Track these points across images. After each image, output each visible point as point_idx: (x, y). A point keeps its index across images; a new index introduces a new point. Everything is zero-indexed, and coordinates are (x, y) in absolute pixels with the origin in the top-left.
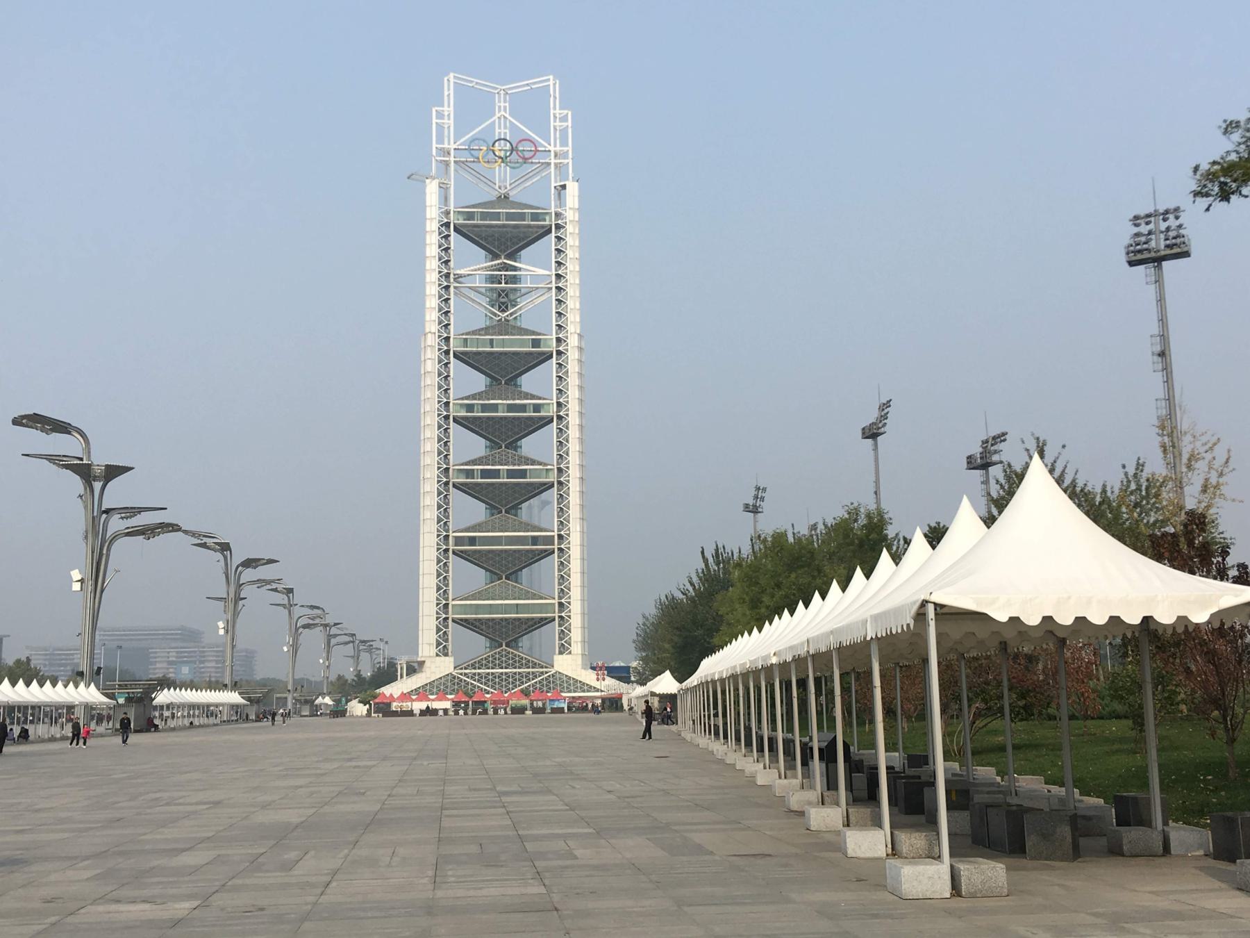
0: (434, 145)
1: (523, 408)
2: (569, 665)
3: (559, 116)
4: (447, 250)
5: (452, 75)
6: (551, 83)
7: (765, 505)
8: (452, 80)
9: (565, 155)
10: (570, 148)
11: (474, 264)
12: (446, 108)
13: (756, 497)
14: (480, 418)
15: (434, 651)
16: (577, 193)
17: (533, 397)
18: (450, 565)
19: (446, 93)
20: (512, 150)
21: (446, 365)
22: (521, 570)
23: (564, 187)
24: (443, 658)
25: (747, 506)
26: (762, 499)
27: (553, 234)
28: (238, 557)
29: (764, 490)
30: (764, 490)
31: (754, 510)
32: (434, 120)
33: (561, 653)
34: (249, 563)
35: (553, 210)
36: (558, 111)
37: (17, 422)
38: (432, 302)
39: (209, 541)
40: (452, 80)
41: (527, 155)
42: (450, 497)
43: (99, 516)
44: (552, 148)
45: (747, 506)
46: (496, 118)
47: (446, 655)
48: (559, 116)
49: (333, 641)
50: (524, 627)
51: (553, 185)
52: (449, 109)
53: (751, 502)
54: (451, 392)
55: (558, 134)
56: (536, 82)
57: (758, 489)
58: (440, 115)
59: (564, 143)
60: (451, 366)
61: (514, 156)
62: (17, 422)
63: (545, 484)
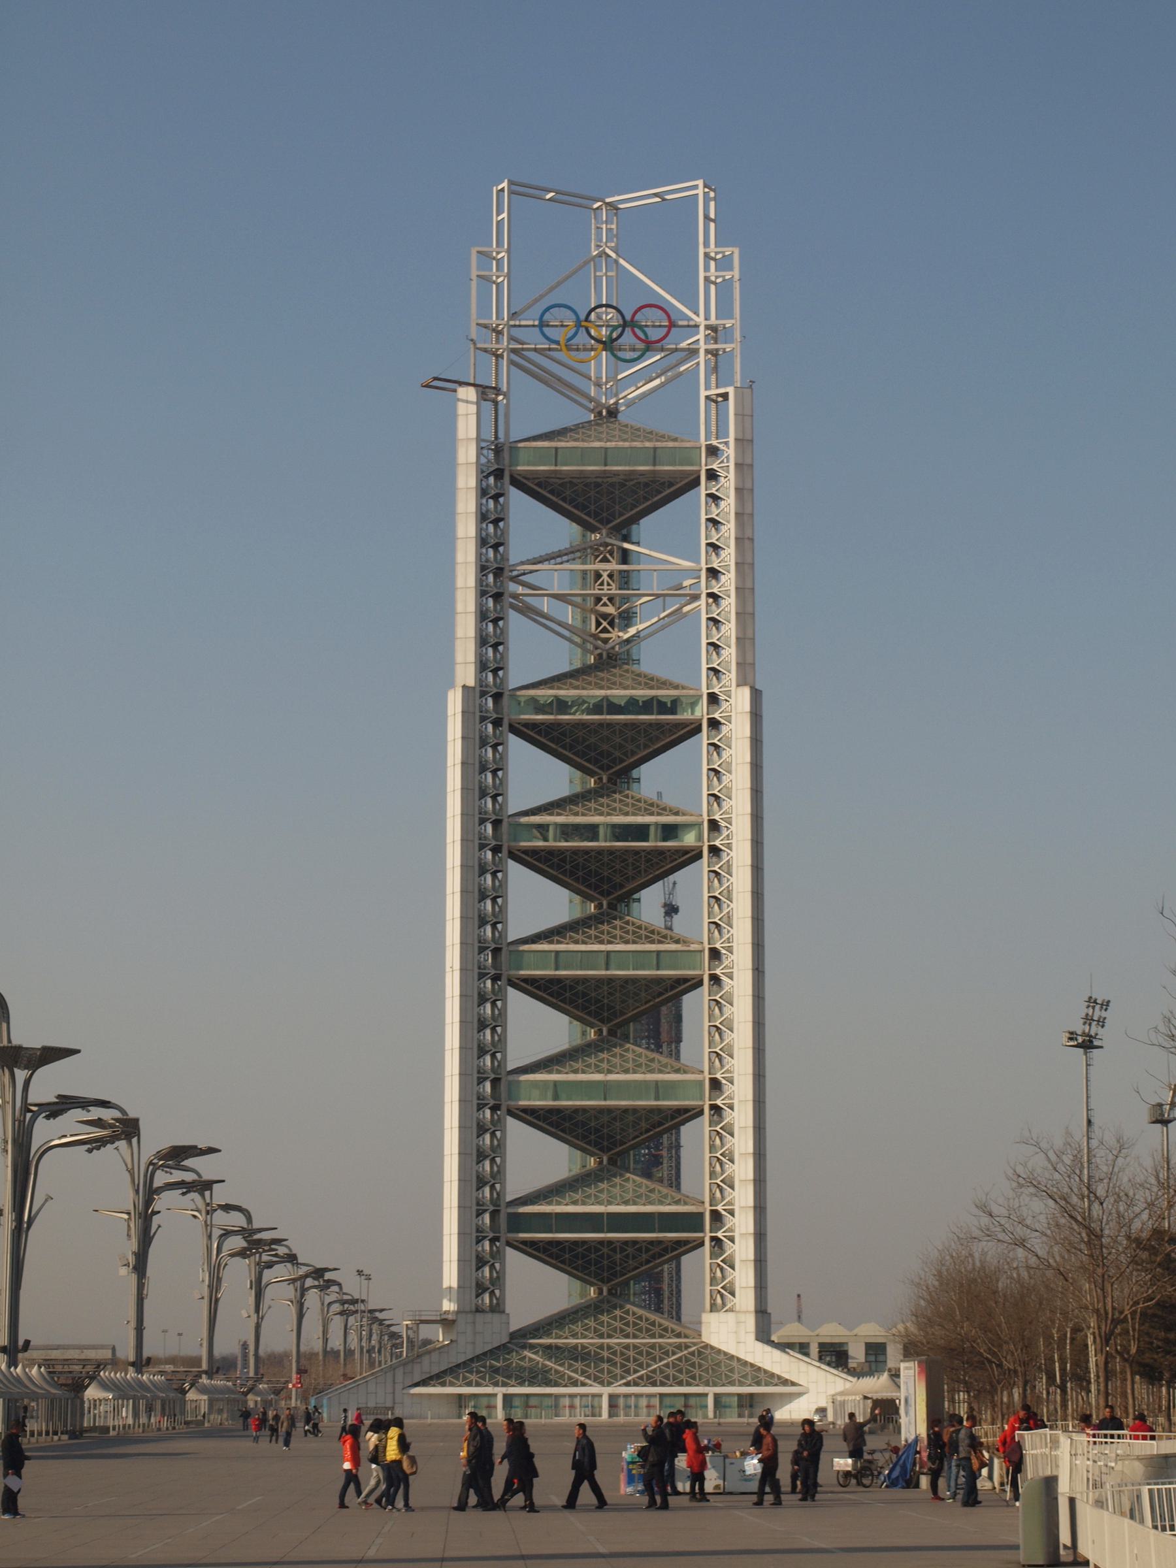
1: (641, 832)
2: (729, 1331)
3: (714, 259)
6: (700, 191)
7: (1105, 1036)
11: (536, 528)
13: (1088, 1020)
14: (561, 852)
17: (664, 810)
20: (625, 325)
25: (1072, 1036)
26: (1101, 1022)
27: (703, 490)
28: (153, 1141)
29: (1106, 1005)
30: (1106, 1005)
31: (1088, 1045)
33: (714, 1308)
34: (177, 1155)
35: (703, 442)
37: (78, 1051)
38: (466, 627)
41: (654, 334)
44: (700, 319)
45: (1072, 1036)
48: (714, 259)
49: (267, 1275)
50: (644, 1256)
51: (703, 393)
53: (1079, 1028)
55: (709, 294)
56: (675, 191)
57: (1092, 1002)
58: (485, 255)
61: (628, 338)
62: (78, 1051)
63: (685, 980)
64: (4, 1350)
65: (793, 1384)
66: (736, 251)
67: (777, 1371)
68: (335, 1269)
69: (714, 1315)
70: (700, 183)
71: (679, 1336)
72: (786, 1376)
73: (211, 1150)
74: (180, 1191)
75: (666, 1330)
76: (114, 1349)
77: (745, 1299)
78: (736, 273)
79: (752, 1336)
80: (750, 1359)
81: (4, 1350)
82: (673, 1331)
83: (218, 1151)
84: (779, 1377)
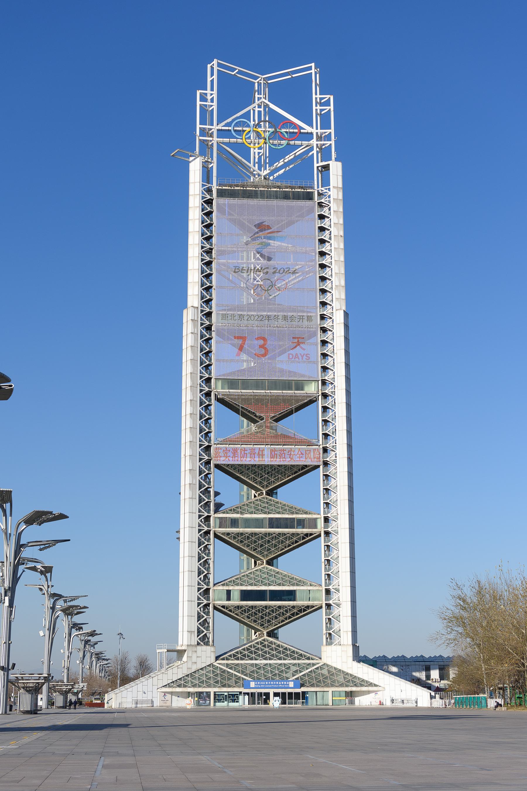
0: (198, 126)
2: (337, 656)
4: (208, 354)
5: (215, 62)
6: (313, 71)
8: (216, 68)
9: (328, 137)
10: (332, 131)
12: (209, 91)
15: (195, 639)
16: (340, 173)
18: (211, 547)
19: (209, 79)
21: (207, 407)
22: (276, 557)
23: (326, 168)
24: (204, 648)
32: (198, 103)
36: (318, 96)
39: (39, 566)
40: (216, 68)
42: (211, 476)
43: (8, 682)
44: (314, 131)
46: (255, 105)
47: (207, 644)
51: (316, 165)
52: (212, 94)
54: (212, 435)
56: (296, 71)
59: (325, 124)
60: (212, 408)
64: (3, 668)
65: (376, 685)
66: (332, 98)
67: (366, 678)
68: (100, 634)
69: (329, 647)
70: (313, 65)
71: (308, 659)
72: (371, 681)
73: (62, 517)
74: (38, 547)
75: (301, 655)
76: (152, 702)
77: (346, 638)
78: (332, 107)
79: (351, 658)
80: (350, 672)
81: (3, 668)
82: (305, 656)
83: (65, 517)
84: (367, 682)
